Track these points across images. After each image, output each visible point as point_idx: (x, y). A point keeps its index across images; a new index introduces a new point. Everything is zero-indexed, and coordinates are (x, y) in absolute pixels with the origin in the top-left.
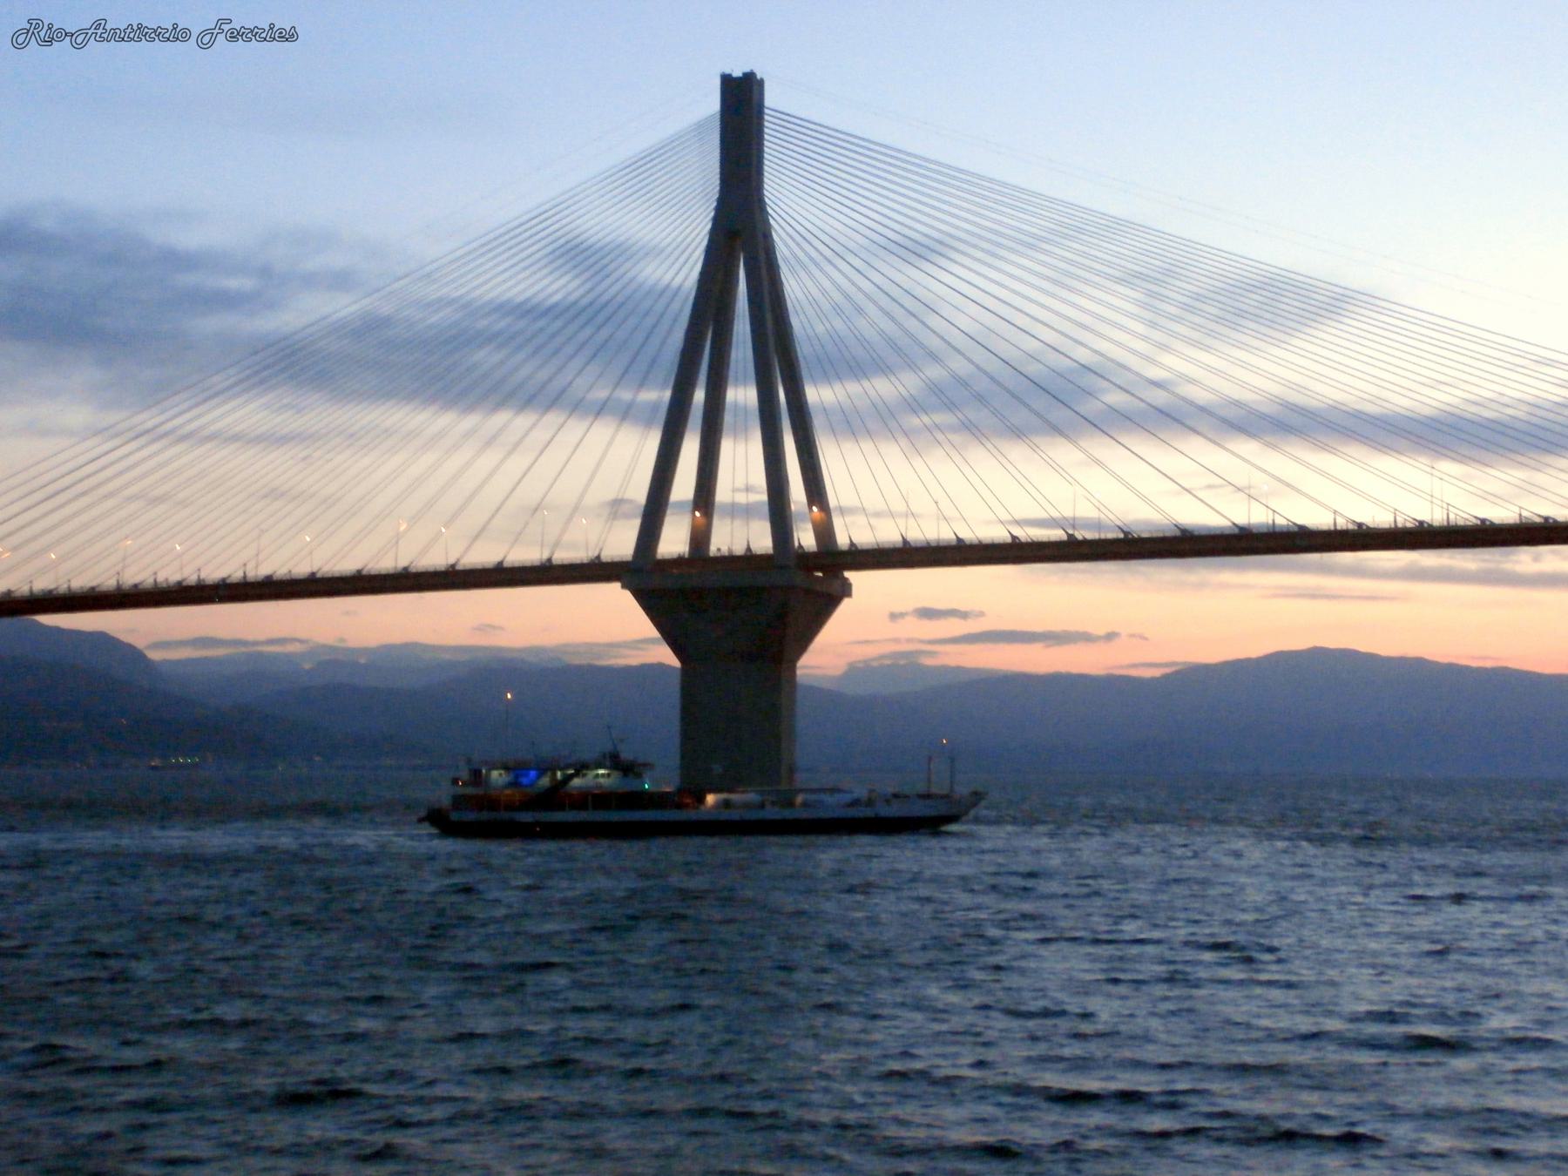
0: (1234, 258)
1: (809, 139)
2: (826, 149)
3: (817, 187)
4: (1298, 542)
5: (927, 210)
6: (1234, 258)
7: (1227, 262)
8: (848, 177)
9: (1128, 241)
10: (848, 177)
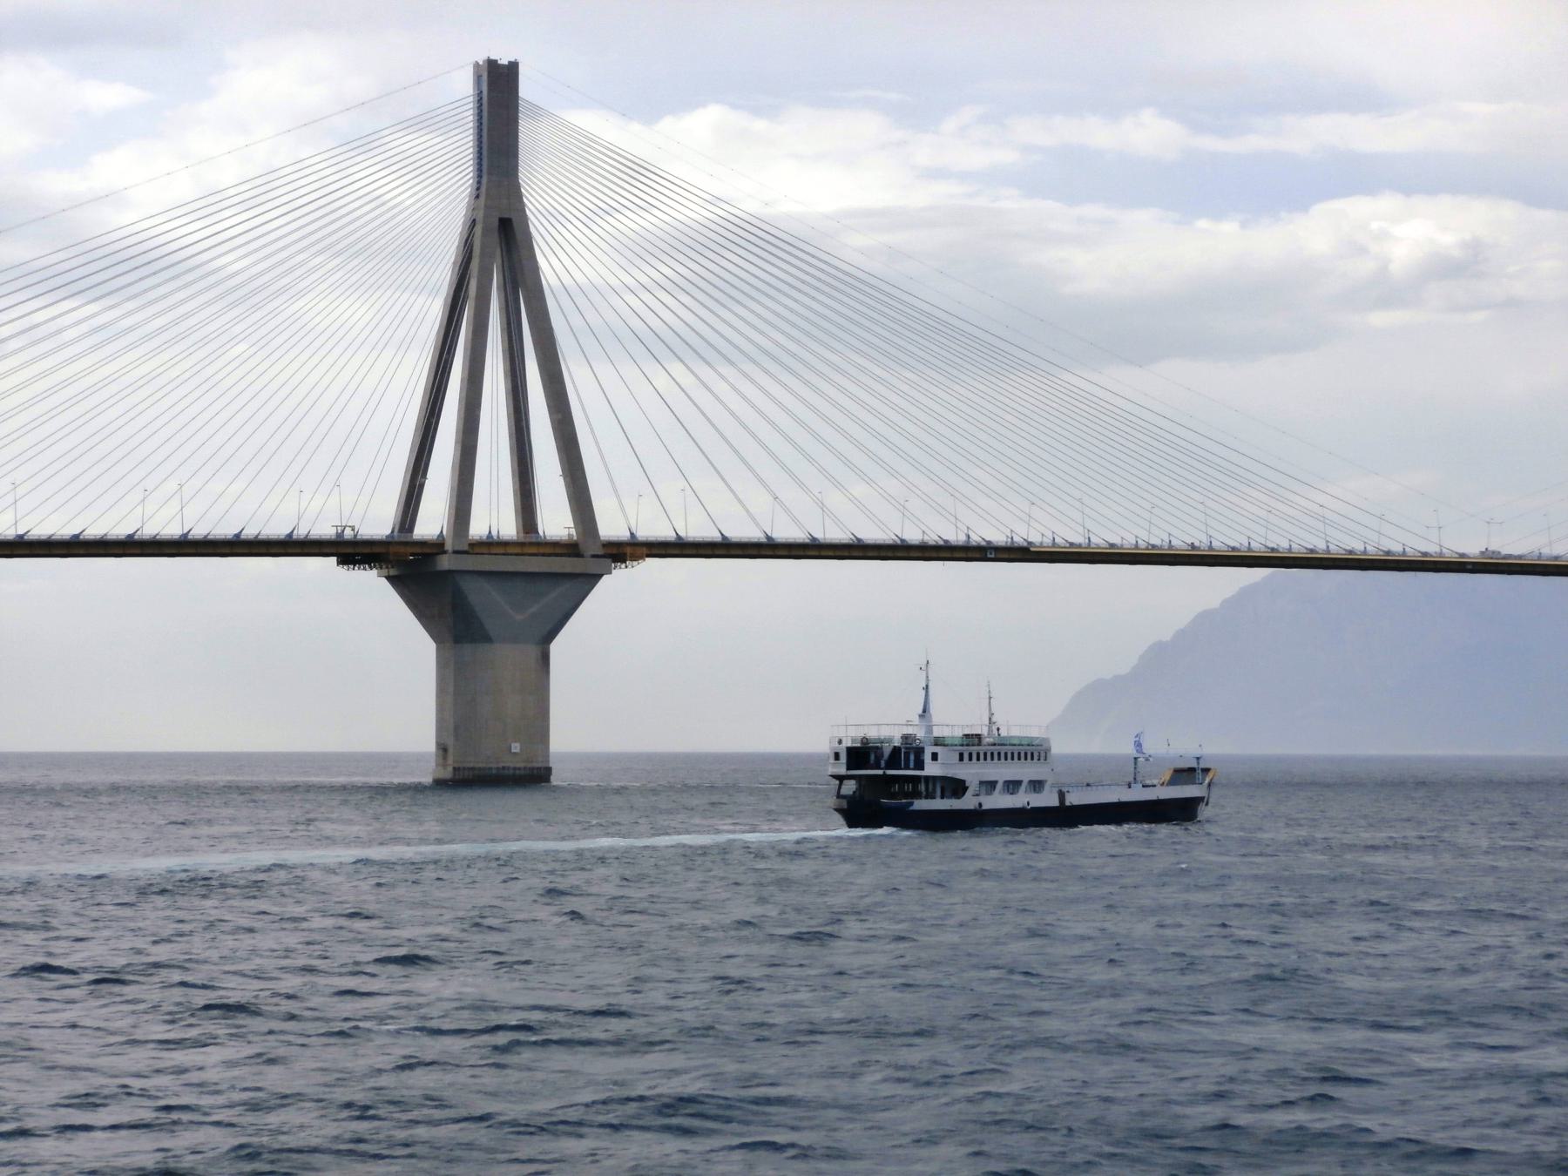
0: (1095, 399)
1: (580, 198)
2: (578, 193)
3: (580, 198)
4: (645, 551)
5: (561, 185)
6: (1095, 399)
7: (1133, 446)
8: (575, 179)
9: (1031, 400)
10: (575, 179)
